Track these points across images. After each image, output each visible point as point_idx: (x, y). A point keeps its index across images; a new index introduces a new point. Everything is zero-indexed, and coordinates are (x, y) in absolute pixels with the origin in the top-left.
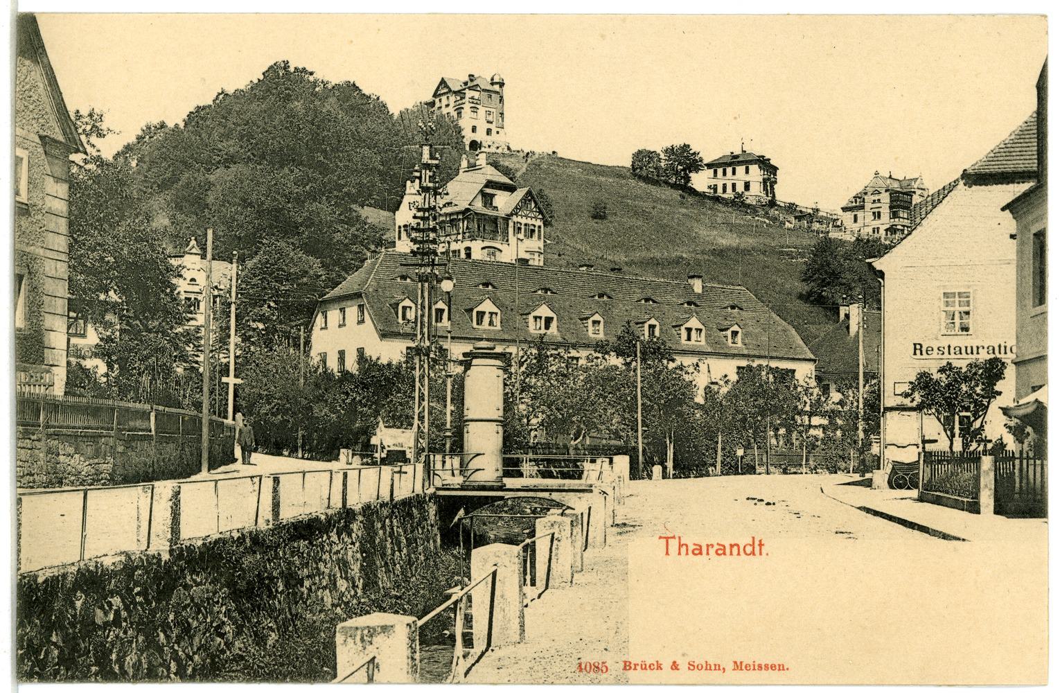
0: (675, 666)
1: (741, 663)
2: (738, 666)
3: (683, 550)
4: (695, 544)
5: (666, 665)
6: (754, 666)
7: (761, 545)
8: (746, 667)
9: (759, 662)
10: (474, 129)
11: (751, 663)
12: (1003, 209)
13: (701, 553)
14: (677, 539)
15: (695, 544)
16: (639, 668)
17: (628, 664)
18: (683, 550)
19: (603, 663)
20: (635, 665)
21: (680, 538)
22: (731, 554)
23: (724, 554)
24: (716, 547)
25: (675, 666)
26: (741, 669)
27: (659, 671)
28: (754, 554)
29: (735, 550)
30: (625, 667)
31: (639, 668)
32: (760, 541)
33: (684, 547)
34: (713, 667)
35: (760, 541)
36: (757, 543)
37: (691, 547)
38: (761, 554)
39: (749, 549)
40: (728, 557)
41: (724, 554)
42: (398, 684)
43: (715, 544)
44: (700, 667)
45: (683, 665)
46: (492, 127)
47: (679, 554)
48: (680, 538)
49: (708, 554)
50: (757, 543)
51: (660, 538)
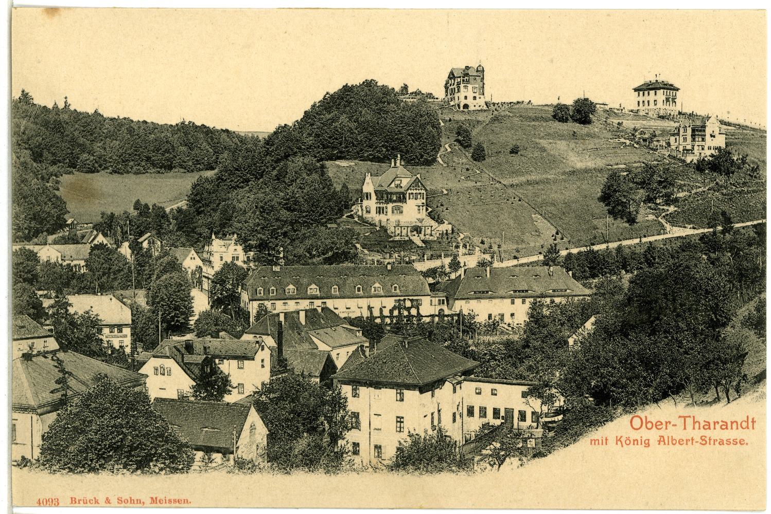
0: (108, 501)
1: (156, 498)
2: (154, 501)
3: (697, 425)
4: (705, 421)
5: (102, 500)
7: (753, 422)
10: (466, 98)
13: (709, 428)
15: (705, 421)
17: (73, 499)
18: (697, 425)
24: (721, 423)
26: (156, 503)
28: (748, 428)
29: (734, 425)
31: (81, 502)
32: (753, 419)
33: (697, 424)
36: (750, 420)
37: (702, 424)
39: (744, 425)
41: (727, 428)
43: (720, 421)
44: (126, 501)
45: (114, 501)
46: (477, 95)
47: (694, 428)
48: (694, 417)
49: (715, 428)
50: (750, 420)
51: (680, 417)
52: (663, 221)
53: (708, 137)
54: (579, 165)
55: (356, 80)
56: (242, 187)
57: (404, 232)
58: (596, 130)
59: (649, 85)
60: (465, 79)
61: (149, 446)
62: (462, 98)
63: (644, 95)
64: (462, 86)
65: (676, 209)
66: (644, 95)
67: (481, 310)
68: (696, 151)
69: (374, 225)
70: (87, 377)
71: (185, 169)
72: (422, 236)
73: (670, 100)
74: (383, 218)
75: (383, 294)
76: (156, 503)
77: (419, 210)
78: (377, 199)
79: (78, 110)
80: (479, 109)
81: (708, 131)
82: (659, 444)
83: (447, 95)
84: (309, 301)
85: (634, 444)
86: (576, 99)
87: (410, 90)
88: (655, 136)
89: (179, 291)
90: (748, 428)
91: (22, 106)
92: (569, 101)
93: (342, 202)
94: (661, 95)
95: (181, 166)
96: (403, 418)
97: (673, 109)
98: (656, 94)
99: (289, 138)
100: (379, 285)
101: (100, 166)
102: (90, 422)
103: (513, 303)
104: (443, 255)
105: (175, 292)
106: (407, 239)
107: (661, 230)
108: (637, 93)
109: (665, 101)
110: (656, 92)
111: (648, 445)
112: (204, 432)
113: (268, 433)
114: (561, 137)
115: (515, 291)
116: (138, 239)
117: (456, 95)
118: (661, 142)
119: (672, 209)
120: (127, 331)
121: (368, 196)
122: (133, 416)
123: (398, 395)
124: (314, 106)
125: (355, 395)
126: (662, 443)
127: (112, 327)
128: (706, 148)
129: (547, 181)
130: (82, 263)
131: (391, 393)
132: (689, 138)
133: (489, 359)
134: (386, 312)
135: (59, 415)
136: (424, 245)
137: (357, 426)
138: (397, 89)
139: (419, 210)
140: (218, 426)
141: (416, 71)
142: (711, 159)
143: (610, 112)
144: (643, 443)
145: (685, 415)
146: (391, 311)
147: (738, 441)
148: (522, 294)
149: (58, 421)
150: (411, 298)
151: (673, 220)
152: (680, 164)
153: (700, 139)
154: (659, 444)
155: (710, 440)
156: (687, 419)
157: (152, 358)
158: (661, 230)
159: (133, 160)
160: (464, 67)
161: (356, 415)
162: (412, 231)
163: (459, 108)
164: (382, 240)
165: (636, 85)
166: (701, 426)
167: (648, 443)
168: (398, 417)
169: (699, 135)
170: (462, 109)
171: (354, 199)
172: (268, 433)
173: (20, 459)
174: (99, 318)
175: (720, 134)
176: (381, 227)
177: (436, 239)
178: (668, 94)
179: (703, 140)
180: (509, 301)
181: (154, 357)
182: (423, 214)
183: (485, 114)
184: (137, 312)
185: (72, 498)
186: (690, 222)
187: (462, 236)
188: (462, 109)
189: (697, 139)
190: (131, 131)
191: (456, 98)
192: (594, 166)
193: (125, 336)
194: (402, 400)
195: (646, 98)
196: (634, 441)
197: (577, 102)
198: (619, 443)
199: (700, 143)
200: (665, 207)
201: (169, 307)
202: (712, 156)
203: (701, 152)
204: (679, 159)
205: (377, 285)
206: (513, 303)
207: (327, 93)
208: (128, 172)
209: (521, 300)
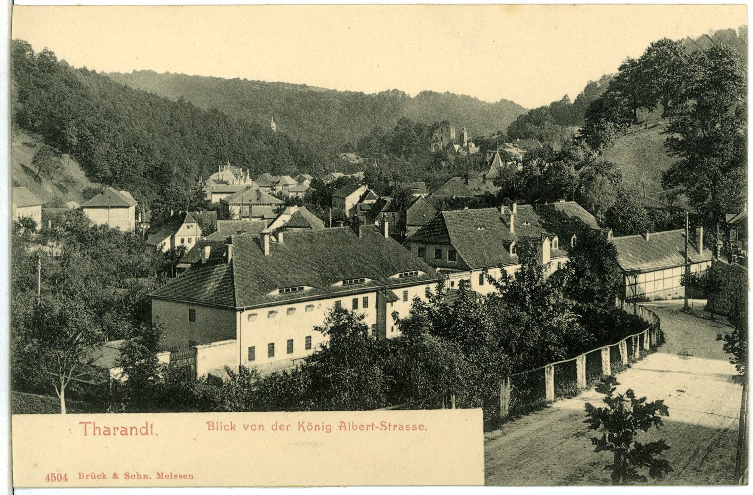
0: (115, 476)
2: (160, 476)
3: (97, 432)
4: (105, 427)
6: (171, 475)
8: (166, 477)
9: (175, 473)
11: (169, 474)
13: (109, 434)
14: (93, 425)
15: (105, 427)
17: (81, 474)
18: (97, 432)
19: (52, 474)
20: (87, 476)
21: (94, 423)
22: (131, 434)
23: (109, 434)
24: (121, 429)
25: (115, 476)
26: (162, 478)
27: (104, 480)
28: (147, 434)
30: (80, 476)
32: (152, 425)
33: (98, 429)
34: (143, 477)
37: (103, 429)
38: (152, 434)
41: (109, 434)
43: (398, 425)
44: (133, 477)
45: (121, 476)
47: (94, 434)
48: (94, 423)
50: (149, 426)
51: (80, 423)
76: (162, 478)
82: (340, 429)
85: (316, 430)
90: (147, 434)
91: (19, 52)
111: (329, 430)
126: (343, 428)
144: (325, 428)
145: (85, 421)
147: (417, 427)
154: (340, 429)
155: (390, 425)
156: (88, 425)
166: (102, 433)
167: (330, 428)
185: (80, 474)
196: (316, 426)
198: (301, 428)
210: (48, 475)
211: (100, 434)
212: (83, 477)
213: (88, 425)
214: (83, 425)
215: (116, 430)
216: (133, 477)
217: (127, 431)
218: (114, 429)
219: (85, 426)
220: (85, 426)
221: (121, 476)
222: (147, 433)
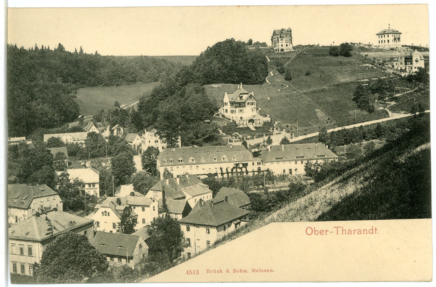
0: (227, 271)
2: (253, 271)
5: (224, 271)
10: (282, 46)
11: (259, 269)
12: (60, 44)
14: (341, 228)
16: (213, 272)
17: (208, 270)
19: (190, 271)
21: (342, 227)
23: (361, 233)
24: (357, 231)
25: (227, 271)
30: (207, 271)
31: (213, 272)
34: (243, 271)
35: (376, 228)
37: (347, 231)
38: (376, 233)
39: (371, 231)
40: (362, 235)
41: (361, 233)
42: (289, 282)
46: (288, 44)
47: (343, 234)
48: (342, 227)
51: (335, 227)
52: (388, 111)
53: (414, 62)
54: (343, 80)
55: (222, 39)
56: (164, 100)
57: (245, 123)
58: (353, 60)
59: (384, 32)
60: (281, 35)
61: (86, 261)
62: (280, 46)
63: (382, 37)
64: (280, 39)
65: (395, 103)
66: (382, 37)
67: (277, 168)
68: (407, 70)
69: (230, 119)
70: (65, 223)
71: (142, 82)
72: (254, 124)
73: (397, 39)
74: (233, 115)
75: (227, 161)
77: (253, 111)
78: (231, 106)
79: (87, 53)
80: (289, 51)
81: (414, 59)
83: (272, 44)
84: (190, 166)
86: (341, 43)
87: (253, 43)
88: (385, 62)
89: (125, 162)
92: (338, 44)
93: (211, 109)
94: (391, 37)
95: (140, 80)
96: (209, 241)
97: (399, 44)
98: (388, 36)
99: (188, 73)
100: (226, 157)
101: (98, 82)
102: (60, 250)
103: (296, 163)
104: (264, 135)
105: (123, 163)
106: (246, 126)
107: (386, 115)
108: (378, 36)
109: (394, 40)
110: (388, 35)
112: (118, 249)
113: (148, 248)
114: (335, 65)
115: (297, 157)
116: (112, 127)
117: (277, 44)
118: (389, 65)
119: (393, 103)
120: (97, 186)
121: (226, 104)
122: (80, 247)
123: (207, 231)
124: (201, 54)
125: (188, 229)
127: (90, 185)
128: (413, 68)
129: (323, 90)
130: (83, 142)
131: (203, 230)
132: (404, 63)
133: (268, 203)
134: (230, 170)
135: (47, 247)
136: (255, 130)
137: (189, 245)
138: (246, 41)
139: (253, 111)
140: (125, 247)
141: (256, 32)
142: (415, 74)
143: (363, 49)
146: (232, 170)
148: (301, 158)
149: (47, 250)
150: (242, 162)
151: (394, 109)
152: (399, 78)
153: (410, 63)
157: (101, 208)
158: (386, 115)
159: (115, 79)
160: (281, 29)
161: (189, 240)
162: (249, 122)
163: (279, 51)
164: (232, 128)
165: (377, 33)
166: (347, 233)
168: (207, 241)
169: (409, 61)
170: (280, 51)
171: (220, 106)
172: (148, 248)
173: (34, 263)
174: (83, 181)
175: (421, 60)
176: (233, 120)
177: (262, 126)
178: (395, 36)
179: (411, 64)
180: (294, 162)
181: (102, 207)
182: (255, 113)
183: (293, 54)
184: (105, 173)
186: (402, 110)
187: (276, 123)
188: (280, 51)
189: (408, 63)
190: (114, 63)
191: (277, 46)
192: (350, 80)
193: (96, 188)
194: (209, 233)
195: (383, 39)
197: (343, 45)
199: (410, 66)
200: (389, 103)
201: (120, 171)
202: (416, 72)
203: (410, 70)
204: (398, 75)
205: (224, 156)
206: (296, 163)
207: (208, 47)
208: (113, 85)
209: (300, 162)
210: (188, 271)
211: (367, 233)
212: (209, 272)
213: (338, 228)
214: (336, 228)
215: (327, 232)
216: (238, 271)
217: (361, 232)
218: (354, 230)
219: (337, 229)
220: (337, 229)
221: (231, 271)
222: (373, 233)
